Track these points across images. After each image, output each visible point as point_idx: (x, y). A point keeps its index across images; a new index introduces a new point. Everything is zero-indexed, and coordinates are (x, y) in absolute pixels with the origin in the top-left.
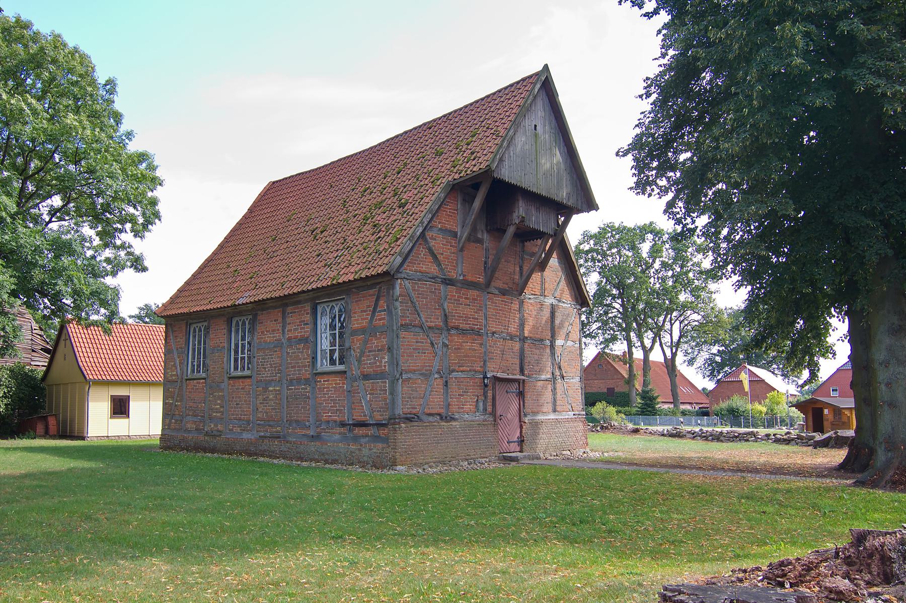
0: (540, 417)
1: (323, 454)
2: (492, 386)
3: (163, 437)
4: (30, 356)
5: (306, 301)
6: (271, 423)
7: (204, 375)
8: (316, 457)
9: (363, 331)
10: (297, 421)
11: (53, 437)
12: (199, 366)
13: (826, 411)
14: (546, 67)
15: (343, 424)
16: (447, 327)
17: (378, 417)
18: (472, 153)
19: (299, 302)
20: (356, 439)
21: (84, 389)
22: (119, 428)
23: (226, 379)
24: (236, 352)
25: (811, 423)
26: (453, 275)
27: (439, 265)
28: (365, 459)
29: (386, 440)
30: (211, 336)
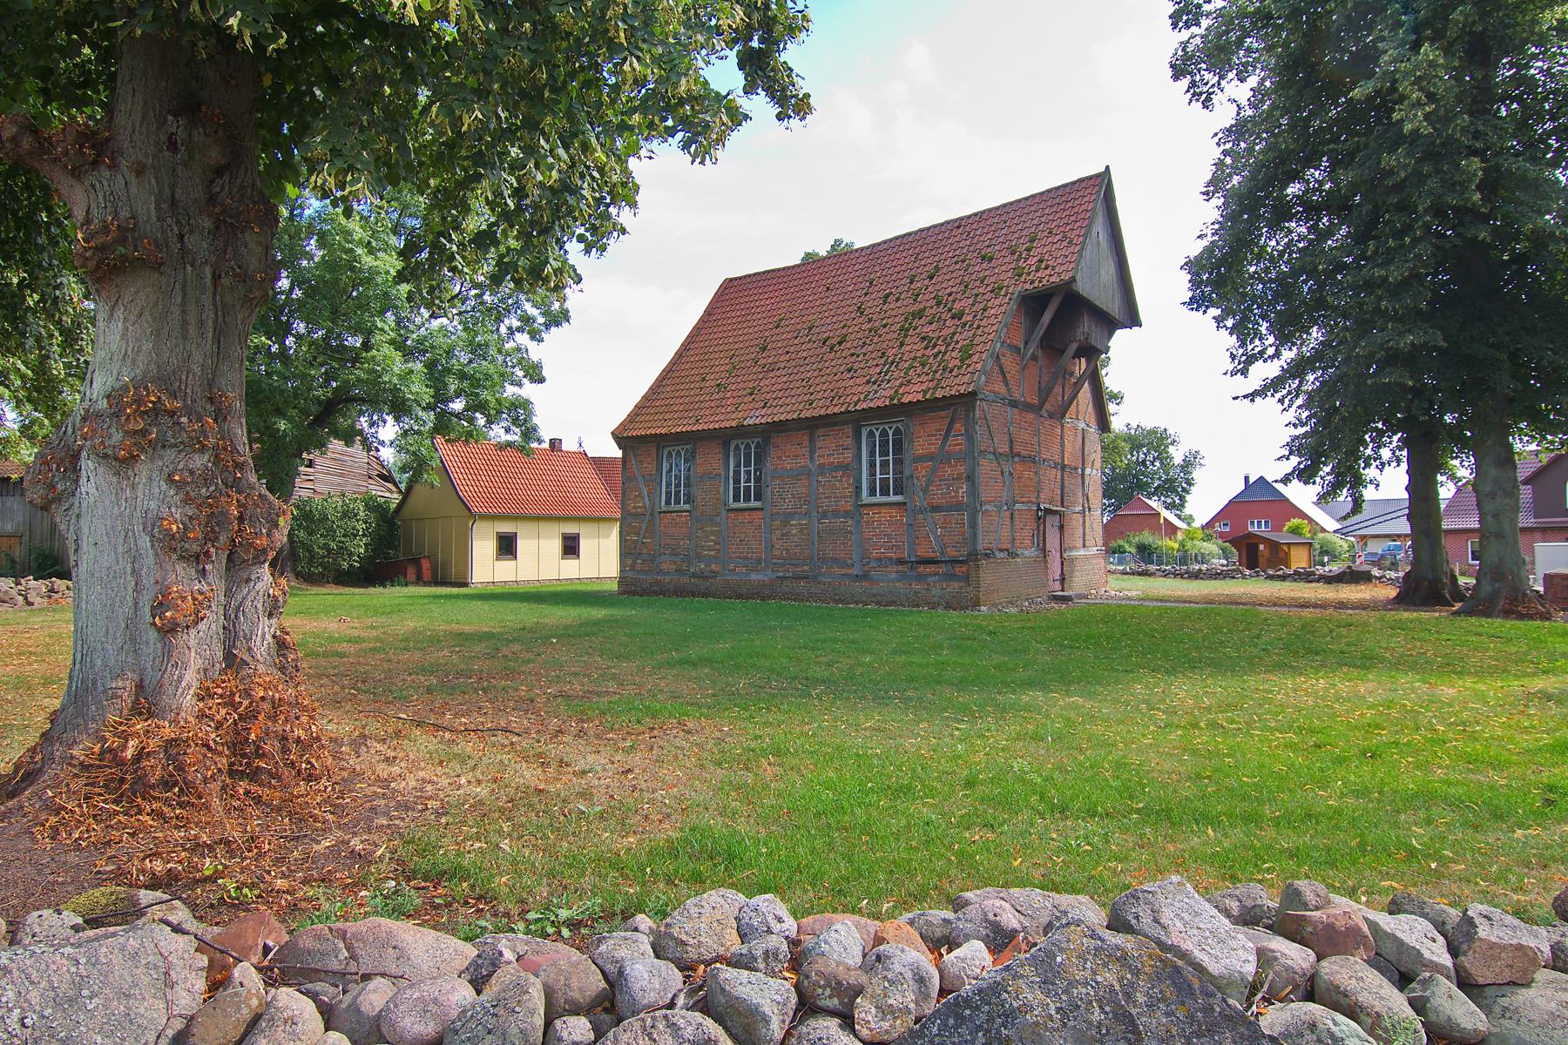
0: (1075, 553)
2: (1042, 516)
3: (622, 580)
5: (845, 423)
7: (687, 507)
9: (931, 457)
10: (834, 559)
12: (677, 493)
13: (1261, 547)
15: (901, 562)
16: (1013, 454)
17: (952, 553)
18: (1041, 261)
19: (836, 424)
22: (571, 570)
23: (724, 513)
24: (737, 481)
26: (1017, 396)
29: (966, 578)
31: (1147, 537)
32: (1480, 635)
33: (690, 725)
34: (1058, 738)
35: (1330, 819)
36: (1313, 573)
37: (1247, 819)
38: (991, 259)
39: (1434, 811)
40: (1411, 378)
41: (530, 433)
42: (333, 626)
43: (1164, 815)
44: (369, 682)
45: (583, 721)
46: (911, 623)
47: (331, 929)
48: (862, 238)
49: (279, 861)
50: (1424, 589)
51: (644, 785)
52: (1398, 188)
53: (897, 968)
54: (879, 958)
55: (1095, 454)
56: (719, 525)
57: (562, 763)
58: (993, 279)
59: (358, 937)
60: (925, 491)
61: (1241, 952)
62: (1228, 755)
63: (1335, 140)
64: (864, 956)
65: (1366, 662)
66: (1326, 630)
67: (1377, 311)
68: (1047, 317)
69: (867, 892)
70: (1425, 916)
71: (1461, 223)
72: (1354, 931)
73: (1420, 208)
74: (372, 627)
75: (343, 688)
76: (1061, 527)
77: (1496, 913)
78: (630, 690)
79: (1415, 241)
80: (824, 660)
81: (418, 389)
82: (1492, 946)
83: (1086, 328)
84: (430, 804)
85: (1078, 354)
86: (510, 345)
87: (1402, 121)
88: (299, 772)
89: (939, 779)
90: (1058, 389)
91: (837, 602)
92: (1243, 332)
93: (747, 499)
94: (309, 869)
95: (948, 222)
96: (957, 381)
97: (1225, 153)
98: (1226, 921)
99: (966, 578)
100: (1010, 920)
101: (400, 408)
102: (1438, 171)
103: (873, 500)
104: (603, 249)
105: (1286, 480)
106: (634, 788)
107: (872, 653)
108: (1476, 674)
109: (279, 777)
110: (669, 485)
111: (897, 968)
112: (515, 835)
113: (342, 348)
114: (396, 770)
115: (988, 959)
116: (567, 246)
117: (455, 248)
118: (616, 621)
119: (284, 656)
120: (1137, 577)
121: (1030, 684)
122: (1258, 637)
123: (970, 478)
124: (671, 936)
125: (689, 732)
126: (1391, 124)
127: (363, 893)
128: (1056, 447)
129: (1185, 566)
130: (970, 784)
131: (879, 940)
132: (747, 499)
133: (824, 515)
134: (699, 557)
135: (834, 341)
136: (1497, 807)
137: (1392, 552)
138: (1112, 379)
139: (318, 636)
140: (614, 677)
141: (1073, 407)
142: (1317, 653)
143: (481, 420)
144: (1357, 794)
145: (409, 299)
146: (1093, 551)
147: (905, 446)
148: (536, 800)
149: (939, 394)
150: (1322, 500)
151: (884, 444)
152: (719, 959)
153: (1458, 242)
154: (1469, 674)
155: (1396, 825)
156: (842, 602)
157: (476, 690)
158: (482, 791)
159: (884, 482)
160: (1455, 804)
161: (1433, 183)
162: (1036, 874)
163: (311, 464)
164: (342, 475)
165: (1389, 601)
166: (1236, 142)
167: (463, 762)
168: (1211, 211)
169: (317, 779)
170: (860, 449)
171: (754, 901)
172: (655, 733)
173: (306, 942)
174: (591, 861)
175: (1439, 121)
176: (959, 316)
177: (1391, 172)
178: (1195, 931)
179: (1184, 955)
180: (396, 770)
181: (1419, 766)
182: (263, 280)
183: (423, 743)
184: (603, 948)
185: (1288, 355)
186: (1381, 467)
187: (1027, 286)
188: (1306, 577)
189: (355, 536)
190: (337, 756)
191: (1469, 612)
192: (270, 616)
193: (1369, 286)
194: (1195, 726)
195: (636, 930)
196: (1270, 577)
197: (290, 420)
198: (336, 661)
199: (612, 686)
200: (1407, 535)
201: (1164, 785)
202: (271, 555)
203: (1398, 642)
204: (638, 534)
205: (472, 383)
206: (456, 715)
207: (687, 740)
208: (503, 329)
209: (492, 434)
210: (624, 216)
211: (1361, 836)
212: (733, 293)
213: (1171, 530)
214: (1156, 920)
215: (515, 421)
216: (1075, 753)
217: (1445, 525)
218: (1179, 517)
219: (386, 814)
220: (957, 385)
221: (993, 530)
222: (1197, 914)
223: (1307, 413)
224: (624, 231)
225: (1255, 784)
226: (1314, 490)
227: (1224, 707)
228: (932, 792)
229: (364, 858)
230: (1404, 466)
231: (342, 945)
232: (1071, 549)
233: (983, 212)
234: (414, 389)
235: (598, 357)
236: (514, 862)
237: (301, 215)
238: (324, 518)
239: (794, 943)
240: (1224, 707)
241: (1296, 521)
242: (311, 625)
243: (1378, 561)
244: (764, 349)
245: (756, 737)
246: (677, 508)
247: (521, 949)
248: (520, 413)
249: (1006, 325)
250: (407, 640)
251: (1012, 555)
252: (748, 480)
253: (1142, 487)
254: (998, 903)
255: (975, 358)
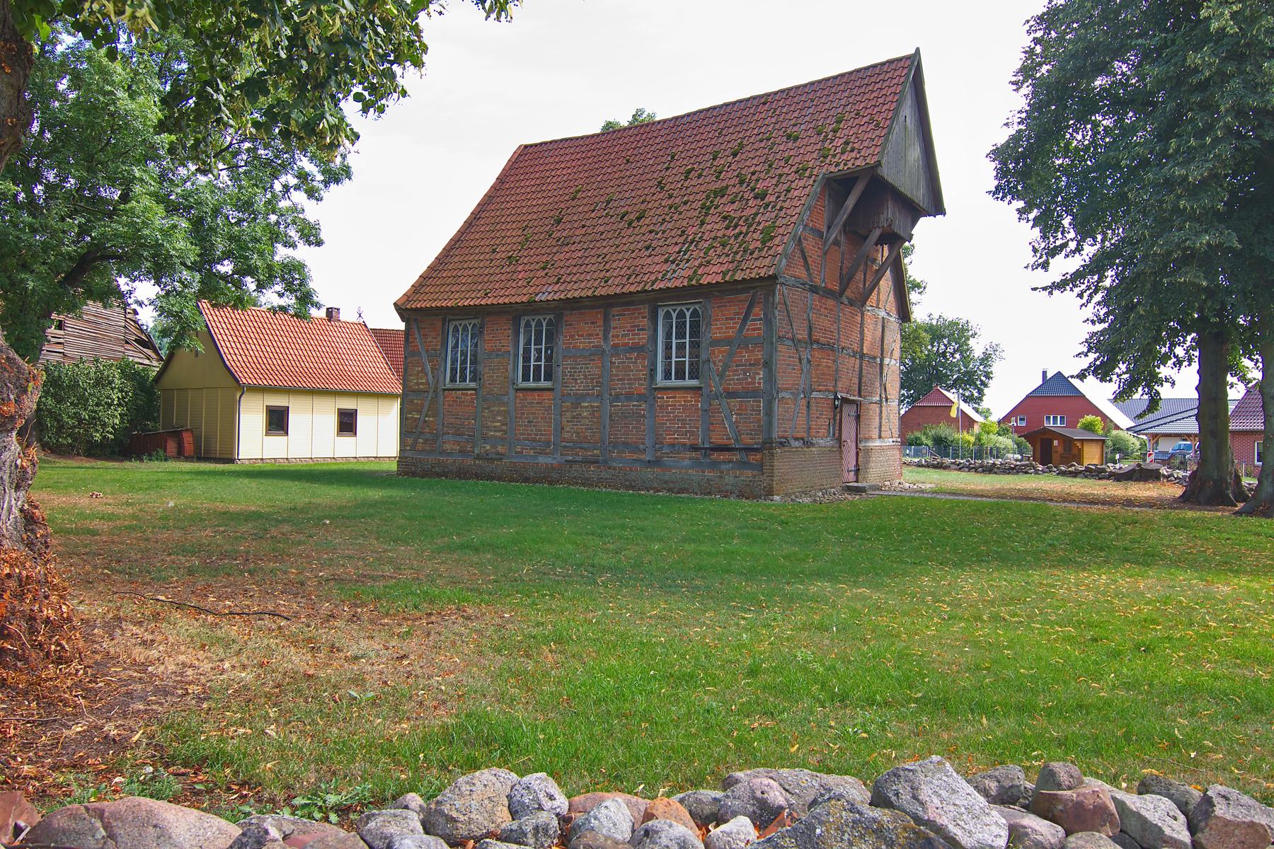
0: (871, 444)
1: (666, 482)
2: (839, 405)
3: (402, 459)
4: (122, 349)
5: (642, 302)
6: (586, 446)
7: (473, 385)
8: (656, 485)
9: (728, 341)
10: (626, 444)
11: (189, 459)
12: (463, 370)
13: (1056, 443)
14: (918, 50)
15: (694, 448)
16: (812, 341)
17: (747, 440)
18: (847, 143)
19: (632, 303)
20: (714, 465)
21: (234, 396)
22: (346, 448)
23: (512, 392)
24: (527, 359)
25: (1038, 455)
26: (818, 281)
27: (808, 270)
28: (729, 487)
29: (760, 467)
30: (487, 337)
31: (944, 430)
32: (1259, 534)
33: (470, 611)
34: (843, 628)
35: (1099, 709)
36: (1104, 470)
37: (1021, 709)
38: (796, 139)
39: (1200, 703)
40: (1206, 278)
41: (306, 298)
42: (84, 501)
43: (941, 705)
44: (127, 561)
45: (356, 606)
46: (702, 511)
47: (87, 809)
48: (664, 110)
49: (25, 746)
50: (1210, 487)
51: (419, 671)
52: (1203, 86)
53: (664, 841)
54: (647, 833)
55: (894, 342)
56: (505, 404)
57: (333, 648)
58: (798, 160)
59: (116, 816)
60: (721, 376)
61: (993, 828)
62: (1008, 648)
63: (1143, 35)
64: (633, 831)
65: (1148, 559)
66: (1112, 527)
67: (1176, 210)
68: (851, 202)
69: (644, 778)
70: (1170, 797)
71: (1261, 125)
72: (1101, 810)
73: (1222, 108)
74: (128, 504)
75: (95, 567)
76: (858, 417)
77: (1234, 793)
78: (408, 574)
79: (1216, 141)
80: (612, 547)
81: (181, 245)
82: (1227, 823)
83: (890, 214)
84: (191, 689)
85: (881, 241)
86: (284, 204)
87: (1209, 18)
88: (48, 654)
89: (722, 667)
90: (859, 276)
91: (628, 488)
92: (1047, 224)
93: (537, 379)
94: (58, 755)
95: (754, 98)
96: (758, 263)
97: (1037, 41)
98: (982, 799)
99: (760, 467)
100: (777, 797)
101: (160, 271)
102: (1241, 72)
103: (668, 383)
104: (381, 110)
105: (1082, 376)
106: (409, 675)
107: (661, 540)
108: (1251, 573)
109: (25, 660)
110: (454, 361)
111: (664, 841)
112: (282, 720)
113: (97, 200)
114: (154, 653)
115: (753, 834)
116: (342, 104)
117: (222, 98)
118: (394, 503)
119: (32, 531)
120: (932, 470)
121: (819, 574)
122: (1046, 532)
123: (768, 364)
124: (442, 813)
125: (468, 618)
126: (1199, 21)
127: (117, 779)
128: (856, 336)
129: (980, 458)
130: (753, 672)
131: (649, 816)
132: (537, 379)
133: (617, 398)
134: (485, 439)
135: (632, 217)
136: (1257, 699)
137: (1182, 451)
138: (915, 268)
139: (67, 512)
140: (391, 561)
141: (874, 296)
142: (1101, 549)
143: (250, 283)
144: (1128, 686)
145: (172, 150)
146: (889, 442)
147: (703, 328)
148: (305, 685)
149: (739, 276)
150: (1121, 397)
151: (681, 326)
152: (490, 834)
153: (1257, 144)
154: (1245, 573)
155: (1162, 716)
156: (632, 487)
157: (242, 572)
158: (247, 676)
159: (680, 366)
160: (1220, 697)
161: (1236, 83)
162: (813, 760)
163: (60, 326)
164: (95, 339)
165: (1175, 500)
166: (1047, 30)
167: (227, 646)
168: (1019, 101)
169: (68, 662)
170: (656, 330)
171: (526, 779)
172: (433, 618)
173: (61, 821)
174: (362, 746)
175: (1245, 20)
176: (762, 196)
177: (1196, 70)
178: (952, 808)
179: (939, 830)
180: (154, 653)
181: (1188, 660)
182: (15, 126)
183: (184, 626)
184: (372, 825)
185: (1089, 250)
186: (1179, 363)
187: (832, 169)
188: (1095, 473)
189: (109, 405)
190: (89, 639)
191: (1250, 512)
192: (18, 488)
193: (1169, 184)
194: (978, 618)
195: (406, 807)
196: (1062, 473)
197: (39, 277)
198: (87, 539)
199: (388, 570)
200: (1196, 435)
201: (943, 676)
202: (20, 423)
203: (1180, 540)
204: (420, 412)
205: (239, 249)
206: (219, 598)
207: (466, 626)
208: (278, 187)
209: (263, 299)
210: (406, 76)
211: (1127, 726)
212: (529, 160)
213: (968, 422)
214: (915, 797)
215: (290, 288)
216: (859, 643)
217: (1232, 426)
218: (977, 410)
219: (143, 699)
220: (758, 268)
221: (789, 417)
222: (954, 791)
223: (1105, 310)
224: (404, 93)
225: (1031, 676)
226: (1111, 388)
227: (1006, 600)
228: (713, 680)
229: (120, 744)
230: (1195, 366)
231: (99, 824)
232: (868, 439)
233: (790, 89)
234: (178, 246)
235: (382, 216)
236: (281, 748)
237: (53, 52)
238: (74, 385)
239: (564, 820)
240: (1006, 600)
241: (1089, 418)
242: (59, 500)
243: (1168, 460)
244: (559, 222)
245: (538, 624)
246: (463, 385)
247: (288, 828)
248: (294, 277)
249: (809, 208)
250: (166, 518)
251: (808, 444)
252: (538, 359)
253: (941, 378)
254: (766, 781)
255: (777, 241)
